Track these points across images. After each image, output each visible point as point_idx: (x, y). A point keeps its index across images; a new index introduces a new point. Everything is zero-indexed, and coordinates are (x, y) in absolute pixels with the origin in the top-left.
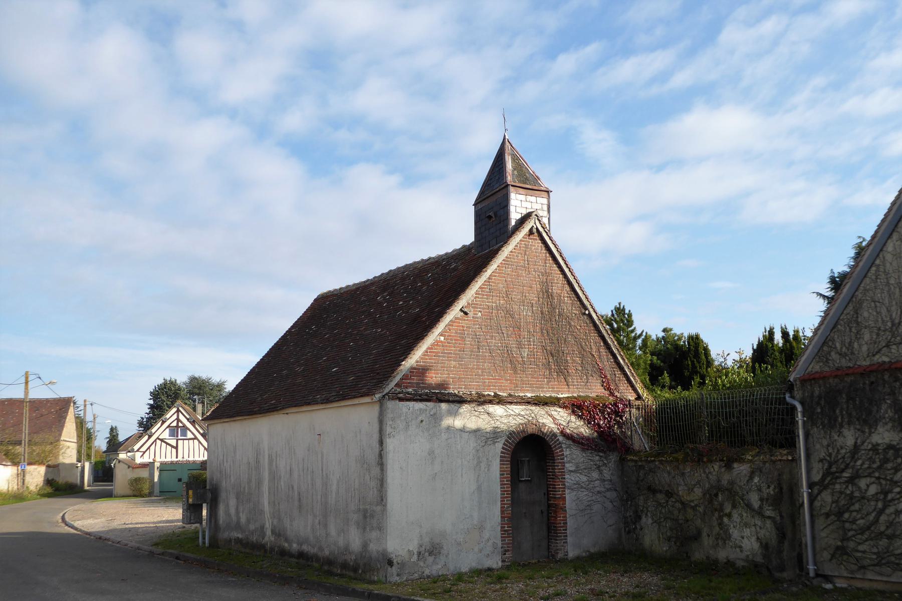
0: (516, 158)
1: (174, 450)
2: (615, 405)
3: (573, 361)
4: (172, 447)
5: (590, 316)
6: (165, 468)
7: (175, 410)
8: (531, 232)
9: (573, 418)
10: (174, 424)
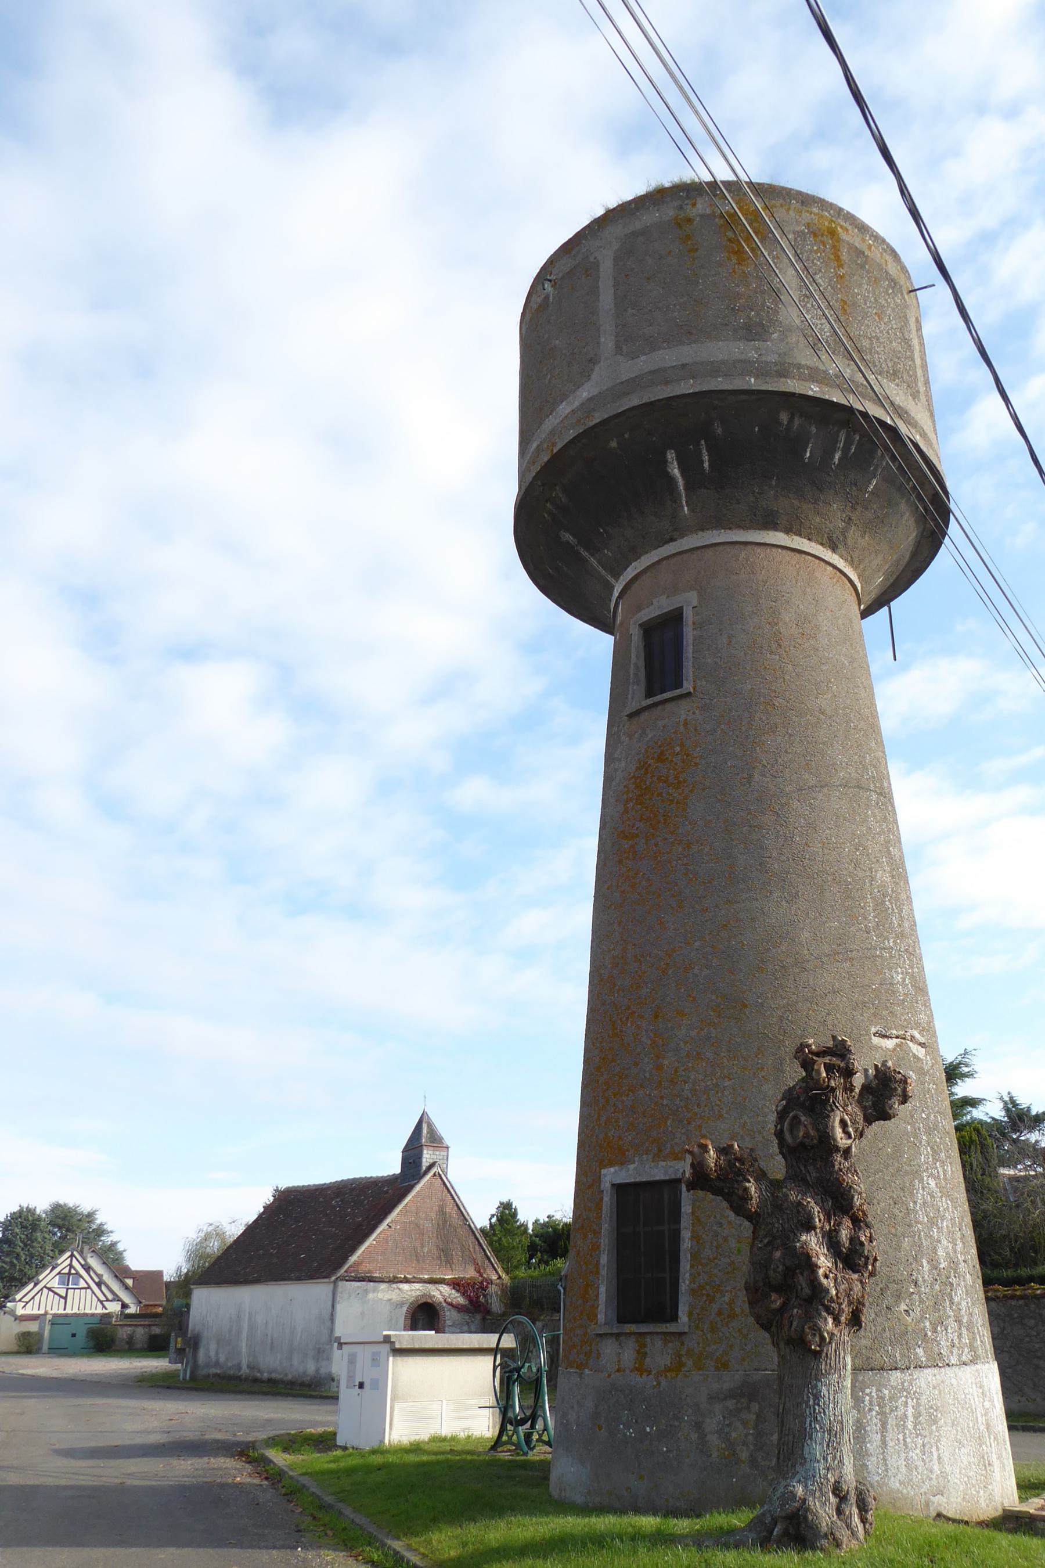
0: (430, 1125)
1: (62, 1301)
2: (482, 1283)
3: (457, 1255)
4: (61, 1297)
5: (469, 1225)
6: (58, 1321)
7: (68, 1254)
8: (435, 1175)
9: (453, 1291)
10: (66, 1271)
